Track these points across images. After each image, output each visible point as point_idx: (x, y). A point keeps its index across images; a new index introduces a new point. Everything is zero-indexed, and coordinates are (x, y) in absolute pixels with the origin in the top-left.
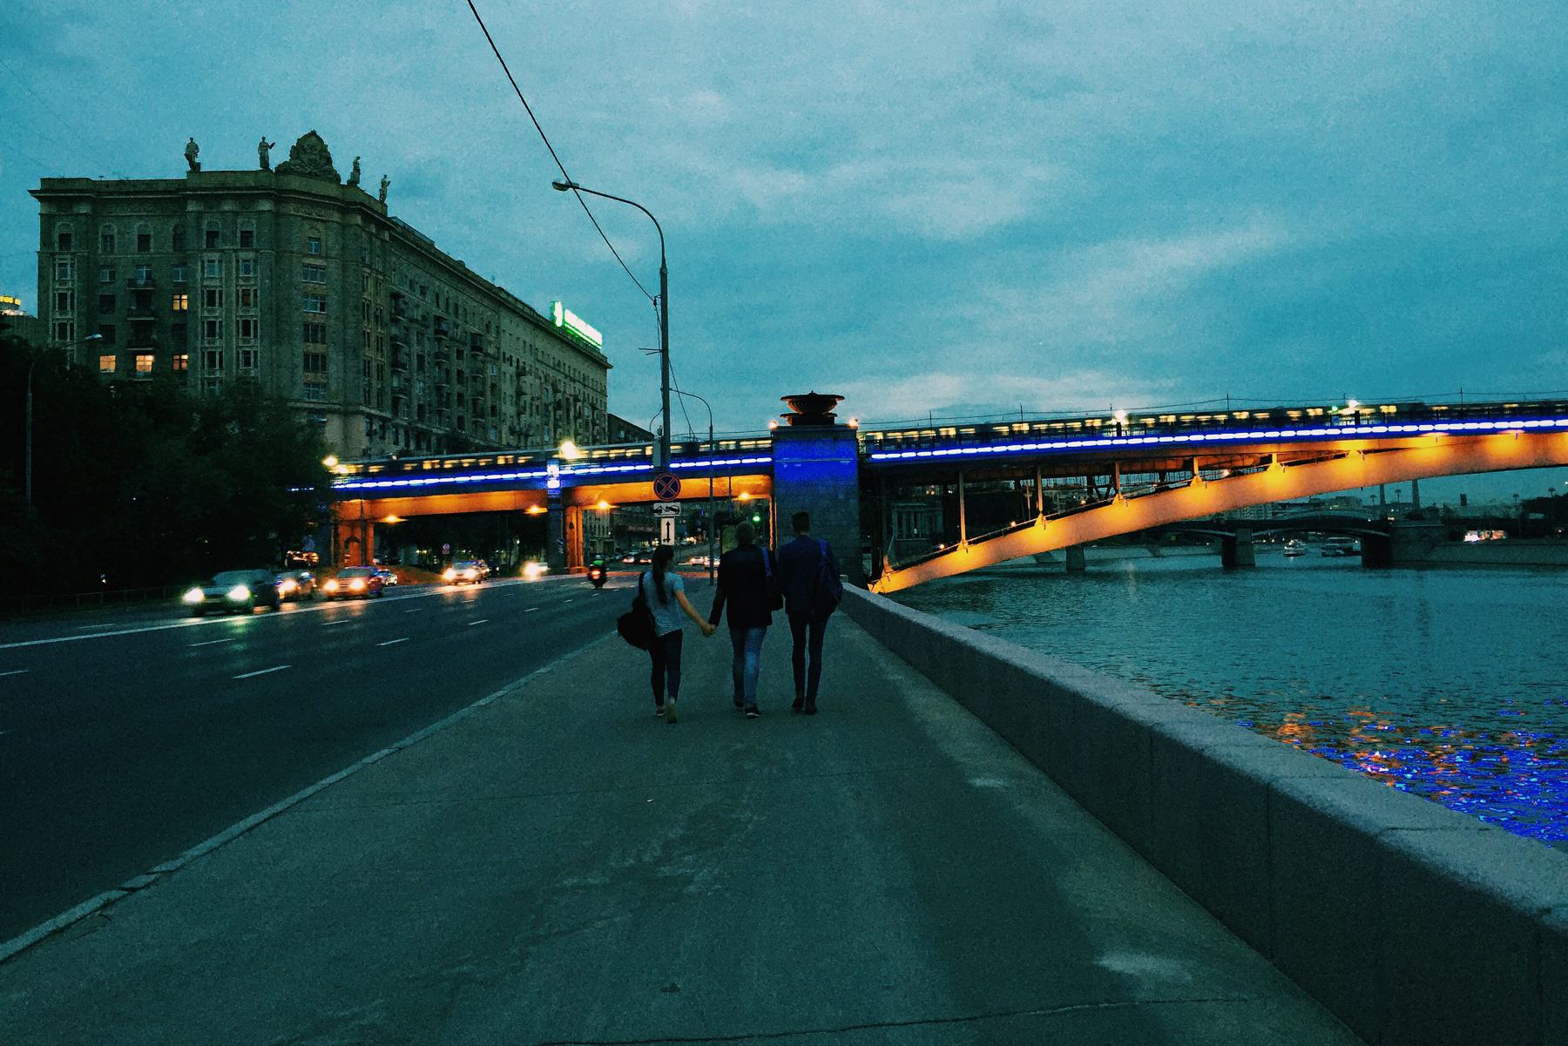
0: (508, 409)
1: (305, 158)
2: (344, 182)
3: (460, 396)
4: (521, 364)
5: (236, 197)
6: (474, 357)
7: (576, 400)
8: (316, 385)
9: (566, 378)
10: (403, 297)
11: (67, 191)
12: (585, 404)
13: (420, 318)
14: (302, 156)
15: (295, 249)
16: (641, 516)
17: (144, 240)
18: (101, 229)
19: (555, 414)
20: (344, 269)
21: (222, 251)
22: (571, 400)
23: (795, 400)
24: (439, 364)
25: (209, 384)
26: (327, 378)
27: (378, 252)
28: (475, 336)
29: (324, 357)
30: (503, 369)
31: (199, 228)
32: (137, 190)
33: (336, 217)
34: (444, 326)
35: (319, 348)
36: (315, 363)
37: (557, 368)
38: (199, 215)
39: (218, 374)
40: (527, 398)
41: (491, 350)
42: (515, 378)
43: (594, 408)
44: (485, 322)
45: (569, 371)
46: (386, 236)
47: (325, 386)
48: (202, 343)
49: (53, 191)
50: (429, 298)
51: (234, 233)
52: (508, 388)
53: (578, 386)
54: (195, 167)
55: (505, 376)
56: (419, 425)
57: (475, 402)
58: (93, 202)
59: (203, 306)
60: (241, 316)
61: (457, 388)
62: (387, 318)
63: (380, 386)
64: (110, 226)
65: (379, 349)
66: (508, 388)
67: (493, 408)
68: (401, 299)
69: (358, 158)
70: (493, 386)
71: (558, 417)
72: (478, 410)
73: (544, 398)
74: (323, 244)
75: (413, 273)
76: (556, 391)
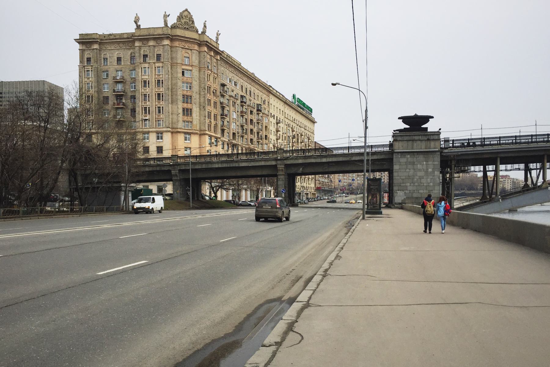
1: (183, 21)
2: (200, 32)
3: (252, 130)
4: (278, 119)
5: (154, 39)
8: (188, 122)
9: (297, 126)
10: (226, 85)
11: (90, 39)
12: (305, 137)
13: (234, 96)
14: (182, 20)
16: (327, 183)
17: (119, 59)
18: (102, 56)
19: (292, 140)
20: (200, 71)
21: (149, 63)
22: (299, 135)
23: (405, 119)
24: (242, 116)
25: (145, 121)
26: (192, 119)
29: (191, 110)
31: (140, 54)
32: (117, 38)
33: (196, 47)
34: (244, 100)
35: (189, 106)
36: (187, 112)
38: (140, 47)
40: (281, 133)
41: (266, 112)
42: (275, 124)
43: (309, 139)
44: (263, 100)
47: (191, 122)
48: (142, 103)
49: (83, 39)
50: (238, 87)
51: (154, 55)
52: (272, 128)
53: (303, 129)
54: (138, 27)
56: (233, 142)
57: (258, 133)
58: (100, 44)
59: (142, 87)
60: (157, 92)
62: (218, 93)
63: (215, 123)
65: (215, 107)
66: (272, 128)
67: (266, 136)
68: (225, 87)
69: (206, 21)
70: (266, 127)
71: (294, 142)
75: (231, 75)
76: (293, 131)
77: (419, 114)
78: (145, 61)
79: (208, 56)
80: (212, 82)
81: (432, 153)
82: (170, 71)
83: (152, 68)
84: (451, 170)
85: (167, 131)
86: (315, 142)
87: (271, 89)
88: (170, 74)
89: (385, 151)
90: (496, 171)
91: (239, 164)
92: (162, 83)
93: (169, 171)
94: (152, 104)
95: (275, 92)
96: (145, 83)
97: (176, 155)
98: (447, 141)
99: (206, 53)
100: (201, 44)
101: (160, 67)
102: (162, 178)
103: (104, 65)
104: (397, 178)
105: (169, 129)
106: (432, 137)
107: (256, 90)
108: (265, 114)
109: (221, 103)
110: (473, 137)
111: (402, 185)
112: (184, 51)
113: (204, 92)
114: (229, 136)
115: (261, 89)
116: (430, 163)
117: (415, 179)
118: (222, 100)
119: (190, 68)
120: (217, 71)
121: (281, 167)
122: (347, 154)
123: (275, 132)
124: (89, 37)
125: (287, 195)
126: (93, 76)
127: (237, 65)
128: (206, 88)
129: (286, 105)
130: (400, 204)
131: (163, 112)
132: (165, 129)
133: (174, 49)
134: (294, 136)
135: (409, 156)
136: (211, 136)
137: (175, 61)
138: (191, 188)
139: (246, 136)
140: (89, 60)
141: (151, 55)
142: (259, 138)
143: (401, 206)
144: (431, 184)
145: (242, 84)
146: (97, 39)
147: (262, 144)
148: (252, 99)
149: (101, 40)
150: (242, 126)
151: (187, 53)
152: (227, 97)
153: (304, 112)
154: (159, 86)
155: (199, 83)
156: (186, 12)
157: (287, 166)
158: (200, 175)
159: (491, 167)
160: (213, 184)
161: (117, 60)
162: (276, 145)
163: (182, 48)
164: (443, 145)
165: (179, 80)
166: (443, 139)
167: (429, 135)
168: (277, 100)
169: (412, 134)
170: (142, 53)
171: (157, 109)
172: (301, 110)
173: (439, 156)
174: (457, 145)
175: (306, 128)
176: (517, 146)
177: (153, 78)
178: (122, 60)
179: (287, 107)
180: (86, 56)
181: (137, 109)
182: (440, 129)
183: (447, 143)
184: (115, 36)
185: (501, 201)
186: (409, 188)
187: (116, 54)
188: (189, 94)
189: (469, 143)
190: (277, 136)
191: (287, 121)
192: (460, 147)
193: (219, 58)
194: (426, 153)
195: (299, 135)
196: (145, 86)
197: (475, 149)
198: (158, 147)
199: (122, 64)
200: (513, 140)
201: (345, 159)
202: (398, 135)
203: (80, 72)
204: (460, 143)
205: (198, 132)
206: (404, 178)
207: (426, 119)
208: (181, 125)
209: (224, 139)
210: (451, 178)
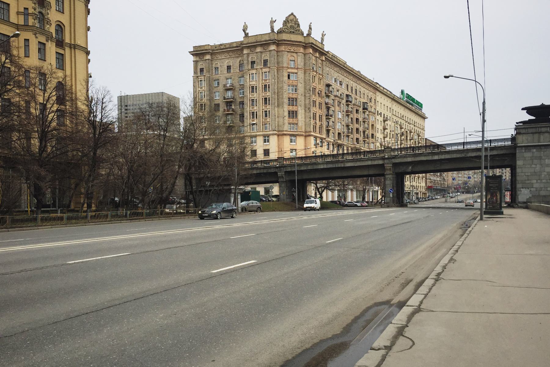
0: (379, 135)
1: (289, 25)
2: (305, 35)
3: (357, 129)
4: (386, 116)
5: (261, 45)
6: (364, 112)
8: (293, 124)
9: (406, 122)
10: (332, 86)
12: (415, 134)
14: (287, 24)
15: (284, 66)
16: (439, 182)
17: (229, 68)
18: (214, 65)
19: (401, 138)
20: (305, 73)
21: (256, 69)
22: (408, 132)
23: (530, 110)
24: (348, 115)
26: (298, 121)
27: (320, 65)
29: (296, 112)
30: (377, 119)
31: (248, 61)
32: (227, 47)
33: (302, 50)
34: (350, 99)
35: (295, 108)
36: (293, 114)
37: (402, 118)
38: (248, 55)
40: (388, 131)
41: (373, 110)
43: (419, 136)
44: (369, 97)
45: (408, 119)
47: (297, 124)
48: (250, 108)
49: (197, 51)
50: (344, 86)
52: (379, 126)
54: (246, 35)
55: (378, 122)
57: (364, 132)
58: (212, 54)
60: (264, 96)
61: (357, 126)
62: (323, 94)
63: (320, 124)
64: (217, 63)
65: (320, 108)
66: (379, 126)
67: (372, 135)
69: (311, 23)
70: (372, 125)
71: (402, 139)
72: (366, 135)
74: (296, 63)
75: (336, 75)
76: (401, 128)
78: (252, 67)
79: (314, 58)
80: (317, 83)
82: (276, 75)
83: (260, 73)
85: (273, 134)
86: (426, 139)
87: (378, 86)
88: (276, 78)
89: (506, 145)
93: (276, 173)
94: (259, 108)
95: (382, 88)
96: (253, 89)
97: (282, 157)
99: (311, 55)
100: (306, 46)
103: (216, 74)
104: (520, 174)
107: (362, 88)
109: (326, 104)
112: (289, 54)
113: (309, 93)
114: (334, 137)
115: (367, 87)
117: (543, 176)
118: (327, 100)
119: (295, 71)
120: (323, 72)
121: (388, 166)
123: (382, 130)
124: (203, 48)
125: (395, 195)
127: (343, 64)
128: (312, 89)
129: (393, 102)
130: (524, 203)
131: (269, 116)
133: (279, 54)
135: (534, 150)
136: (316, 137)
137: (281, 65)
138: (297, 189)
139: (351, 136)
140: (202, 70)
142: (366, 137)
143: (526, 206)
147: (368, 143)
150: (348, 126)
151: (293, 56)
152: (332, 97)
153: (413, 108)
154: (265, 90)
156: (292, 16)
157: (395, 165)
158: (305, 177)
160: (319, 185)
162: (383, 144)
163: (288, 52)
165: (285, 83)
168: (384, 97)
169: (539, 126)
170: (250, 60)
171: (264, 112)
175: (415, 125)
177: (260, 84)
178: (232, 68)
180: (199, 67)
181: (245, 114)
184: (225, 46)
187: (226, 63)
190: (384, 134)
191: (395, 118)
193: (324, 59)
195: (408, 132)
196: (253, 92)
198: (265, 150)
199: (232, 72)
201: (459, 156)
203: (194, 82)
205: (304, 134)
206: (529, 174)
209: (329, 140)
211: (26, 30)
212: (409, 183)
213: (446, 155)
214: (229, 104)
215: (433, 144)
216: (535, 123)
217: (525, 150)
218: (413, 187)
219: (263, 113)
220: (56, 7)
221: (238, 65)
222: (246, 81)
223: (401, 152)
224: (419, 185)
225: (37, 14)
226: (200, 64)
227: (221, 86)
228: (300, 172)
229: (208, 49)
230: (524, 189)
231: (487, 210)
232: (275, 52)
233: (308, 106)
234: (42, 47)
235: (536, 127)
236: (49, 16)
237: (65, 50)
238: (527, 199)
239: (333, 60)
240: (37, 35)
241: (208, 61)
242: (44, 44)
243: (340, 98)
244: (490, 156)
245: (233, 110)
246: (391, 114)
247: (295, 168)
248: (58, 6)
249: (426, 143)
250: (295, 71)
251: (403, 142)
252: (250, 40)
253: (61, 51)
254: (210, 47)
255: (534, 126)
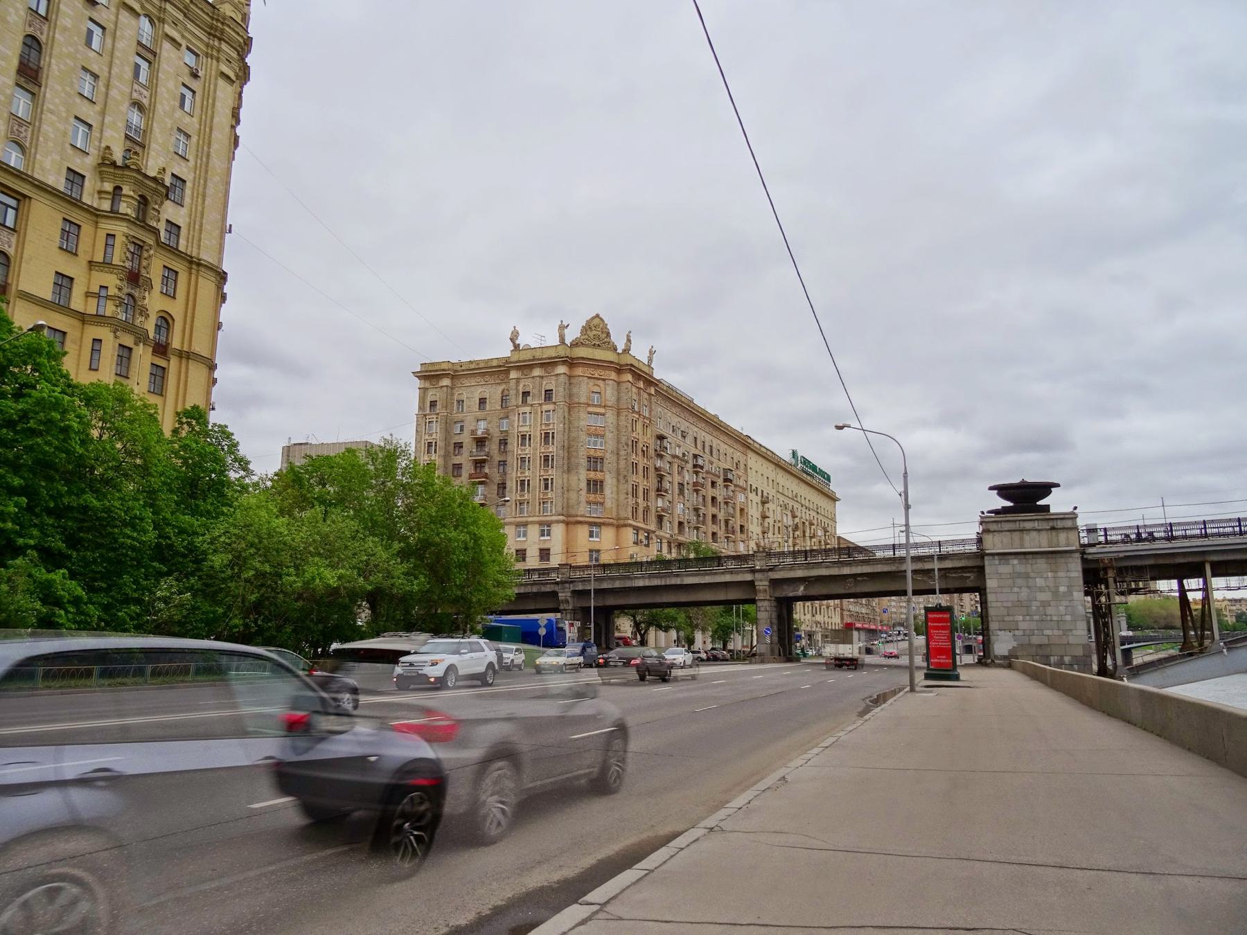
1: (591, 334)
2: (620, 351)
3: (714, 516)
4: (765, 494)
5: (542, 365)
7: (811, 524)
8: (596, 503)
10: (666, 438)
13: (681, 455)
17: (482, 401)
18: (456, 397)
20: (618, 414)
21: (532, 405)
22: (807, 523)
23: (1003, 491)
24: (697, 491)
27: (646, 403)
28: (726, 471)
29: (602, 482)
31: (517, 390)
32: (480, 366)
33: (613, 375)
34: (700, 462)
35: (599, 476)
36: (595, 486)
38: (518, 380)
39: (526, 497)
40: (770, 521)
41: (741, 483)
43: (826, 531)
44: (735, 461)
46: (652, 391)
47: (602, 504)
49: (427, 371)
50: (689, 440)
52: (754, 512)
54: (516, 347)
56: (679, 538)
57: (727, 522)
60: (543, 453)
62: (652, 452)
66: (754, 512)
69: (630, 332)
70: (742, 510)
72: (730, 528)
73: (785, 520)
74: (603, 397)
75: (675, 420)
76: (794, 517)
77: (1030, 479)
78: (524, 402)
79: (634, 390)
80: (641, 433)
81: (1054, 556)
82: (566, 417)
83: (537, 413)
84: (1107, 587)
85: (558, 522)
86: (839, 538)
87: (749, 441)
88: (567, 422)
89: (967, 551)
90: (1206, 589)
91: (683, 581)
92: (553, 437)
93: (554, 594)
94: (534, 474)
95: (758, 446)
97: (567, 564)
98: (1092, 530)
99: (630, 385)
100: (620, 370)
101: (549, 411)
102: (539, 606)
103: (457, 413)
104: (994, 604)
105: (561, 518)
106: (1060, 524)
107: (722, 444)
108: (740, 487)
109: (657, 469)
110: (1148, 522)
111: (1007, 619)
112: (591, 382)
114: (672, 529)
115: (730, 442)
116: (1061, 574)
117: (1034, 608)
118: (659, 463)
119: (602, 410)
120: (650, 415)
121: (762, 583)
122: (890, 559)
123: (760, 518)
124: (437, 367)
125: (776, 639)
126: (438, 431)
127: (686, 401)
128: (630, 443)
129: (779, 470)
130: (1005, 657)
131: (552, 488)
132: (554, 518)
133: (574, 381)
134: (797, 525)
135: (1016, 562)
136: (637, 529)
138: (593, 624)
139: (703, 528)
141: (536, 391)
142: (729, 529)
143: (1008, 662)
144: (1068, 618)
145: (695, 434)
146: (449, 370)
147: (734, 542)
148: (715, 461)
149: (456, 371)
150: (696, 510)
152: (668, 458)
153: (814, 482)
154: (547, 442)
155: (618, 434)
157: (775, 583)
158: (611, 601)
159: (1193, 583)
160: (638, 618)
161: (480, 403)
162: (762, 544)
163: (589, 378)
164: (1086, 539)
166: (1084, 528)
167: (1053, 519)
168: (761, 460)
169: (1019, 518)
170: (521, 391)
171: (542, 482)
172: (809, 478)
173: (1080, 560)
174: (1114, 538)
175: (819, 511)
176: (1206, 542)
178: (488, 402)
179: (781, 473)
180: (429, 398)
181: (508, 484)
182: (1075, 508)
183: (1093, 535)
184: (478, 364)
185: (1226, 653)
186: (1022, 625)
187: (477, 393)
188: (599, 454)
189: (1139, 534)
190: (763, 527)
191: (782, 498)
192: (1123, 542)
193: (653, 392)
194: (1050, 556)
195: (807, 523)
196: (523, 444)
197: (1154, 547)
198: (541, 550)
199: (487, 409)
200: (1233, 527)
202: (991, 522)
203: (417, 425)
204: (1121, 535)
205: (615, 522)
206: (1010, 604)
207: (1045, 489)
208: (583, 510)
209: (662, 534)
210: (1110, 605)
211: (99, 324)
212: (803, 614)
213: (864, 567)
214: (479, 465)
215: (851, 546)
216: (1015, 513)
217: (1000, 559)
218: (819, 625)
219: (540, 483)
220: (162, 288)
221: (498, 397)
222: (513, 426)
223: (795, 558)
224: (830, 620)
225: (123, 297)
226: (430, 393)
227: (466, 433)
228: (599, 592)
229: (447, 368)
230: (1003, 632)
231: (929, 672)
232: (567, 378)
233: (623, 472)
234: (126, 354)
235: (1015, 521)
236: (146, 301)
237: (169, 361)
238: (1010, 651)
239: (669, 394)
240: (118, 334)
241: (445, 389)
242: (130, 349)
243: (681, 460)
244: (940, 570)
245: (486, 476)
246: (774, 491)
247: (590, 584)
248: (167, 285)
249: (839, 544)
250: (602, 410)
251: (798, 541)
252: (527, 356)
253: (162, 363)
254: (450, 366)
255: (1012, 519)
